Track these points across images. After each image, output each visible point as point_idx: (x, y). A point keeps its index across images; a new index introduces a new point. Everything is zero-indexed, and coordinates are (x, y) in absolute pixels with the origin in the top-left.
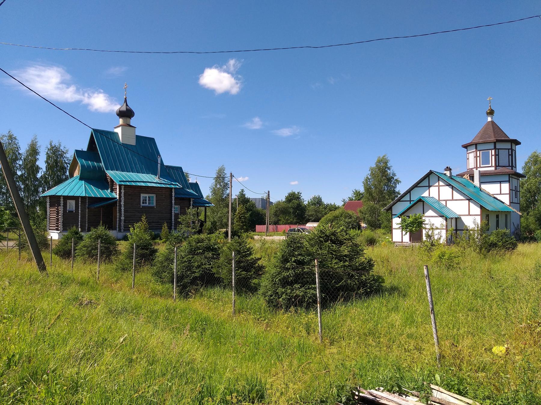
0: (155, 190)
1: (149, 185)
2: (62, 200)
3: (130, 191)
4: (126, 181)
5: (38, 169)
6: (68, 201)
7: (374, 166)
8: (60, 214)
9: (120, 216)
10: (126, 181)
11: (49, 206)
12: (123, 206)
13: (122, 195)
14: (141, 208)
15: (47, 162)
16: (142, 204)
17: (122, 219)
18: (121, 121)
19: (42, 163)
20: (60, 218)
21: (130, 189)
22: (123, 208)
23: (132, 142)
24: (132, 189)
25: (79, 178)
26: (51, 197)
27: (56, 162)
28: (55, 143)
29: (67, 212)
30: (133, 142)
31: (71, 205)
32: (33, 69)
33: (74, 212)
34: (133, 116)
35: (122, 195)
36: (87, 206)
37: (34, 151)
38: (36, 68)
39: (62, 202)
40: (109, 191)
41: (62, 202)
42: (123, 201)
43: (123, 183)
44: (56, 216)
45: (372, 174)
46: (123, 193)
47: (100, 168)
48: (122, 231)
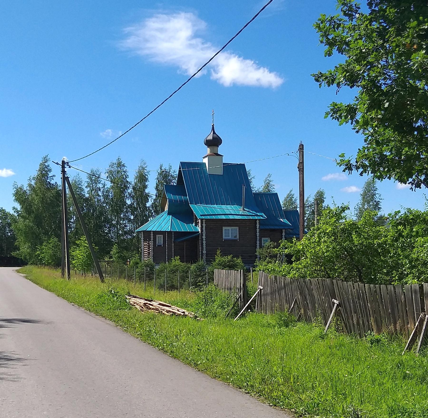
0: (238, 222)
1: (231, 217)
2: (152, 234)
4: (217, 215)
5: (146, 197)
8: (150, 248)
9: (202, 249)
12: (204, 240)
13: (204, 229)
15: (157, 188)
16: (224, 237)
20: (150, 252)
22: (204, 242)
23: (220, 172)
25: (167, 213)
28: (166, 167)
29: (157, 246)
31: (160, 240)
32: (154, 19)
34: (221, 143)
35: (204, 229)
36: (173, 240)
38: (157, 17)
39: (152, 237)
40: (194, 224)
41: (152, 237)
42: (204, 235)
43: (203, 217)
44: (148, 251)
46: (204, 227)
47: (186, 201)
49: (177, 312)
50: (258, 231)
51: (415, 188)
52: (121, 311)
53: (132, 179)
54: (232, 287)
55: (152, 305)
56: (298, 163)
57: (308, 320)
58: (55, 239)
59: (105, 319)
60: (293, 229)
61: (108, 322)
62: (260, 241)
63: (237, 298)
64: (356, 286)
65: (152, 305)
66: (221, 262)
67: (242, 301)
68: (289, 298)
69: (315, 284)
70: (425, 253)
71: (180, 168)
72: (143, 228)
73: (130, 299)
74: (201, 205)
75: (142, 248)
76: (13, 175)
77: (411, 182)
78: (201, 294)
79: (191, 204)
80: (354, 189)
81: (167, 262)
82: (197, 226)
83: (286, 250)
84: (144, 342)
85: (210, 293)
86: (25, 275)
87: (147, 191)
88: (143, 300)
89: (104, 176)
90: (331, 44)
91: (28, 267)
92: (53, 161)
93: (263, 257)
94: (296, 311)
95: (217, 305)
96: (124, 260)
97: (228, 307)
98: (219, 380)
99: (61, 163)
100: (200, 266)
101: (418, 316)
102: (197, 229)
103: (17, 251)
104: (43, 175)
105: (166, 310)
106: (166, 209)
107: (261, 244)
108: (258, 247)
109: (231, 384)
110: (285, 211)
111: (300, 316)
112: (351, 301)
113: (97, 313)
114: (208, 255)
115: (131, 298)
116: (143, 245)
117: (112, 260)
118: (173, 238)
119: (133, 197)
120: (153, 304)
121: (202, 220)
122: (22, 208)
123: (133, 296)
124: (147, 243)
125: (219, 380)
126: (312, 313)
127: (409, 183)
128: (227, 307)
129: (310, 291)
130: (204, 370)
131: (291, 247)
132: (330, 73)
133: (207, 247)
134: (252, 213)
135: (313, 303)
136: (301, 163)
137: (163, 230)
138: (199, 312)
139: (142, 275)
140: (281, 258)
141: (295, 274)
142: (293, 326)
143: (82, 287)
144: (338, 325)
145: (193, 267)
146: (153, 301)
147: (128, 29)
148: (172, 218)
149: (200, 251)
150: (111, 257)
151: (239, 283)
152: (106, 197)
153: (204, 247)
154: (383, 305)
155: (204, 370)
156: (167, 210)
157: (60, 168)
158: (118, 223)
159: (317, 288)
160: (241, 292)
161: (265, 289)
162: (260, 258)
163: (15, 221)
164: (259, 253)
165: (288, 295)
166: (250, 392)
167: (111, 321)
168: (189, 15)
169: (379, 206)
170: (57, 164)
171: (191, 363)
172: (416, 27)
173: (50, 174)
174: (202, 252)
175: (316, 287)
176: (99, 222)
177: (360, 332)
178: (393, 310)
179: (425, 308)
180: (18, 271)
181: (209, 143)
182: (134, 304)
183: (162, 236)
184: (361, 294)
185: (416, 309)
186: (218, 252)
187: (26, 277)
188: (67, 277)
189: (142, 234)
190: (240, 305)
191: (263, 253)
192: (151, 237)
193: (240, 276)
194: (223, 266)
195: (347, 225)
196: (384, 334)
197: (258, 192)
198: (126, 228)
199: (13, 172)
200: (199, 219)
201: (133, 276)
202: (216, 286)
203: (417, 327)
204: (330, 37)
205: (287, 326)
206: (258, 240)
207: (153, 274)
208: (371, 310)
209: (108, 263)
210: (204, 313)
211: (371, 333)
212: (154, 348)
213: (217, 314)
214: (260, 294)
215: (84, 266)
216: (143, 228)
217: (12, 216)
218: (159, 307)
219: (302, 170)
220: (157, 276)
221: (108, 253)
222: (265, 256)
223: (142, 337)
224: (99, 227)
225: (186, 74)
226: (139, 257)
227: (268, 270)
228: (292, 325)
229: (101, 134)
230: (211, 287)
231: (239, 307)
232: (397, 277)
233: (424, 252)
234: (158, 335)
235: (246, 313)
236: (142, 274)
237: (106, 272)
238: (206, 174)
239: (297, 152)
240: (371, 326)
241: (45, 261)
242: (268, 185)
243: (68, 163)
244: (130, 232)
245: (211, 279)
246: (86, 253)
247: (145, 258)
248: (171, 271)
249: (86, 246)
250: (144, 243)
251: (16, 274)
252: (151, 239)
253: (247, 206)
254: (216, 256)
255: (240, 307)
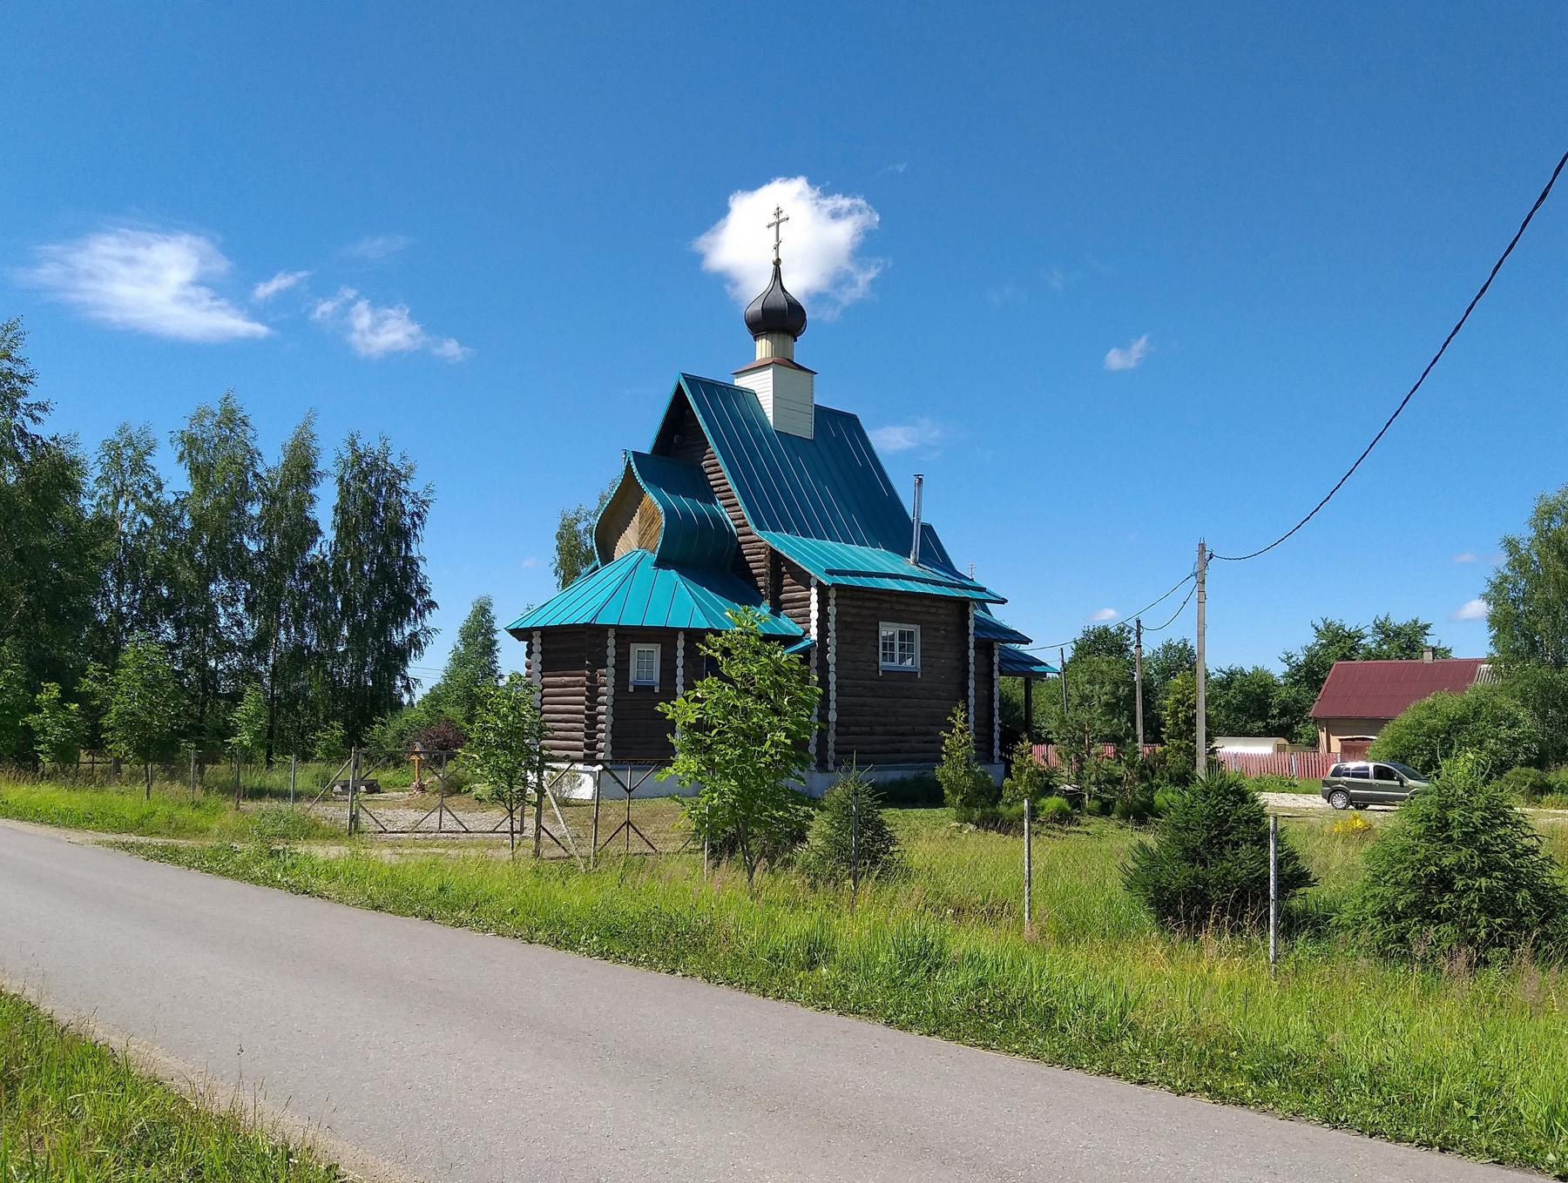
3: (853, 611)
6: (635, 649)
7: (1525, 533)
12: (832, 668)
14: (880, 679)
16: (881, 663)
18: (763, 348)
19: (324, 508)
21: (848, 602)
24: (855, 603)
27: (370, 509)
28: (370, 442)
29: (631, 689)
30: (805, 428)
32: (110, 239)
33: (657, 690)
37: (302, 469)
39: (611, 652)
41: (611, 652)
42: (832, 649)
44: (587, 708)
45: (1520, 563)
48: (831, 766)
124: (584, 675)
168: (201, 243)
183: (656, 650)
192: (608, 650)
250: (546, 679)
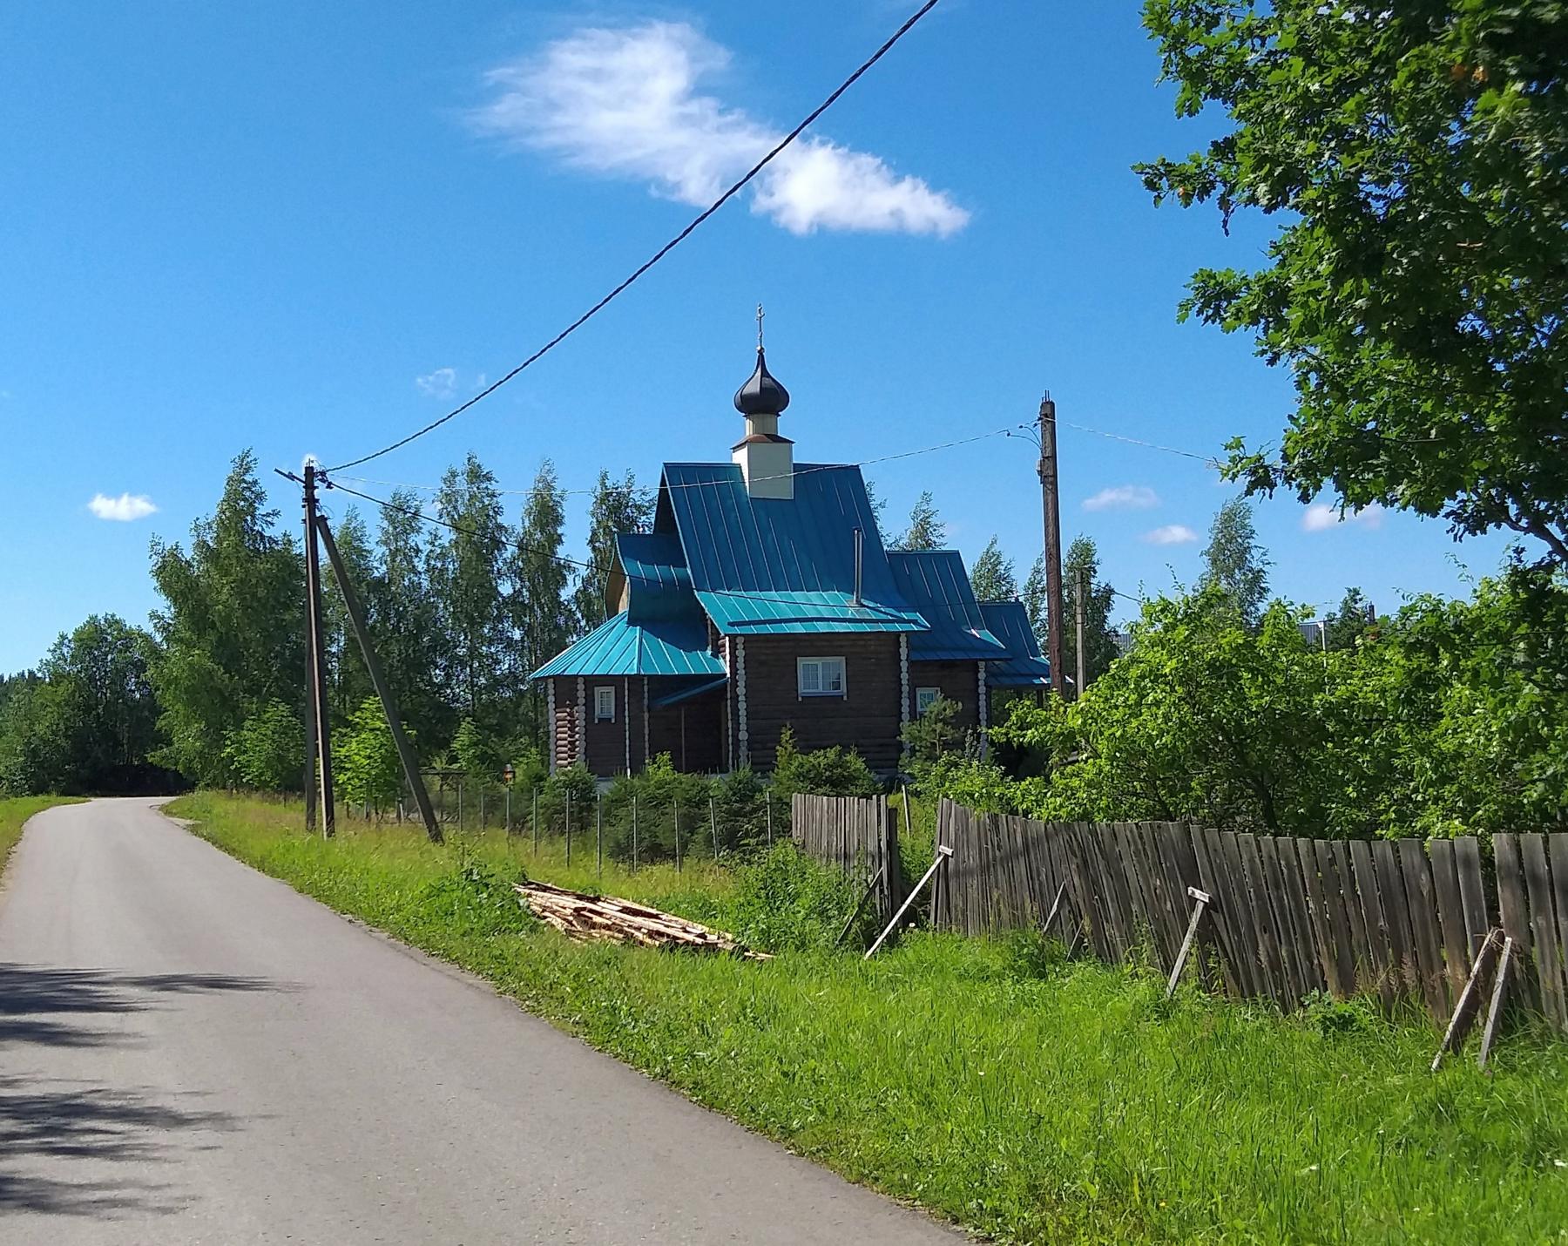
1: (822, 628)
2: (581, 687)
4: (764, 622)
8: (577, 729)
9: (737, 729)
10: (764, 622)
11: (554, 706)
12: (741, 698)
13: (740, 665)
16: (802, 689)
17: (740, 738)
22: (742, 706)
25: (626, 619)
26: (558, 679)
28: (616, 479)
29: (596, 721)
31: (605, 703)
32: (574, 43)
33: (613, 721)
35: (740, 665)
37: (547, 514)
38: (584, 38)
39: (581, 694)
40: (709, 652)
41: (581, 694)
42: (741, 684)
43: (737, 630)
44: (569, 736)
46: (741, 660)
47: (685, 583)
49: (681, 934)
50: (904, 669)
51: (1464, 532)
52: (506, 937)
53: (514, 517)
54: (852, 852)
55: (600, 914)
56: (1040, 458)
57: (1107, 956)
58: (281, 708)
59: (461, 968)
60: (1011, 660)
61: (471, 981)
62: (913, 698)
63: (868, 885)
64: (1266, 845)
65: (600, 914)
66: (806, 767)
67: (886, 893)
68: (1040, 884)
69: (1130, 840)
70: (1479, 735)
71: (663, 483)
72: (552, 667)
73: (530, 895)
74: (731, 592)
75: (552, 728)
76: (153, 515)
77: (1453, 512)
78: (752, 873)
79: (698, 591)
80: (1178, 533)
81: (629, 770)
82: (718, 658)
83: (1030, 731)
84: (599, 1050)
85: (782, 868)
86: (189, 822)
87: (561, 552)
88: (569, 898)
89: (431, 509)
90: (1196, 75)
91: (198, 795)
92: (276, 470)
93: (921, 746)
94: (1067, 924)
95: (806, 906)
96: (494, 764)
97: (839, 914)
98: (875, 1188)
99: (301, 474)
100: (739, 784)
101: (1479, 940)
102: (720, 667)
103: (162, 748)
104: (239, 515)
105: (646, 931)
106: (624, 606)
107: (913, 705)
108: (905, 716)
109: (919, 1203)
110: (985, 607)
111: (1080, 941)
112: (1252, 894)
113: (429, 948)
114: (756, 746)
115: (534, 892)
116: (552, 721)
117: (455, 766)
118: (646, 695)
119: (519, 574)
120: (604, 911)
121: (733, 638)
122: (179, 614)
123: (538, 885)
125: (875, 1188)
126: (1120, 931)
127: (1447, 516)
128: (836, 913)
129: (1113, 861)
130: (818, 1151)
131: (1046, 721)
132: (1195, 164)
133: (751, 722)
134: (885, 613)
135: (1124, 900)
136: (1047, 458)
137: (615, 671)
138: (748, 932)
139: (555, 816)
140: (975, 750)
141: (1061, 806)
142: (1059, 975)
143: (377, 861)
144: (1207, 970)
145: (715, 781)
146: (599, 900)
147: (497, 74)
148: (641, 634)
149: (730, 733)
150: (453, 759)
151: (876, 839)
152: (437, 575)
153: (743, 720)
154: (1358, 906)
155: (821, 1153)
156: (627, 610)
157: (299, 491)
158: (473, 652)
159: (1137, 852)
160: (880, 866)
161: (961, 857)
162: (913, 751)
163: (154, 651)
164: (908, 736)
165: (1039, 875)
166: (993, 1235)
167: (480, 977)
168: (680, 30)
169: (1262, 585)
170: (291, 477)
171: (770, 1127)
172: (1481, 11)
173: (262, 510)
174: (735, 737)
175: (1132, 848)
176: (414, 651)
177: (1283, 993)
178: (1392, 919)
179: (1501, 913)
180: (167, 811)
181: (748, 405)
182: (543, 911)
183: (612, 689)
184: (1285, 871)
185: (1470, 917)
186: (786, 735)
187: (194, 830)
188: (325, 829)
189: (551, 686)
190: (878, 906)
191: (923, 734)
193: (879, 815)
194: (812, 781)
195: (1227, 648)
196: (1363, 997)
197: (897, 549)
198: (497, 667)
199: (151, 504)
200: (726, 635)
201: (529, 818)
202: (799, 848)
203: (1476, 976)
204: (1192, 53)
205: (1042, 976)
206: (905, 695)
207: (590, 809)
208: (1319, 923)
209: (445, 776)
210: (766, 934)
211: (1320, 997)
212: (636, 1069)
213: (808, 938)
214: (943, 873)
215: (374, 791)
216: (552, 667)
217: (147, 638)
218: (624, 920)
219: (1050, 479)
220: (604, 816)
221: (445, 744)
222: (929, 744)
223: (589, 1033)
224: (421, 666)
225: (675, 198)
226: (539, 757)
227: (972, 796)
228: (1057, 970)
229: (420, 380)
230: (782, 851)
231: (876, 912)
232: (1394, 811)
233: (1477, 731)
234: (640, 1023)
235: (903, 932)
236: (556, 812)
237: (441, 806)
238: (745, 500)
239: (1036, 425)
240: (1318, 973)
241: (249, 777)
242: (924, 527)
243: (323, 474)
244: (514, 678)
245: (785, 828)
246: (380, 748)
247: (561, 759)
248: (650, 802)
249: (378, 729)
251: (160, 821)
252: (579, 702)
253: (868, 592)
254: (778, 748)
255: (879, 914)
